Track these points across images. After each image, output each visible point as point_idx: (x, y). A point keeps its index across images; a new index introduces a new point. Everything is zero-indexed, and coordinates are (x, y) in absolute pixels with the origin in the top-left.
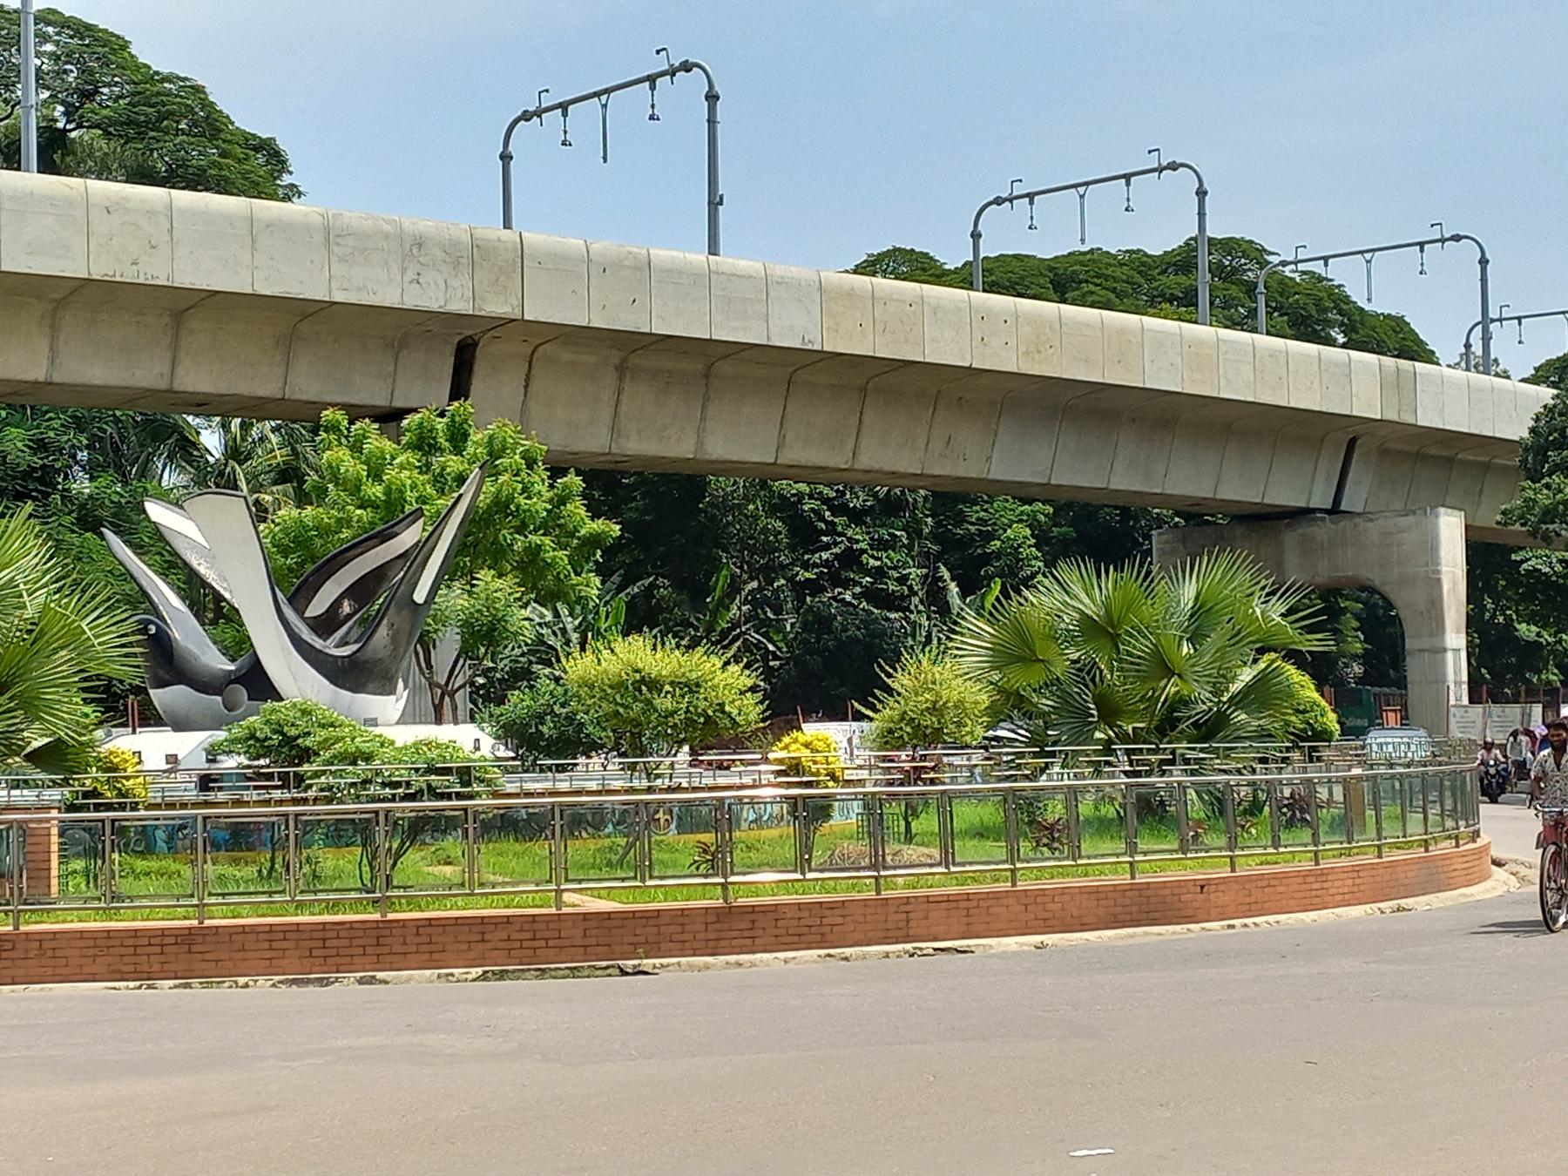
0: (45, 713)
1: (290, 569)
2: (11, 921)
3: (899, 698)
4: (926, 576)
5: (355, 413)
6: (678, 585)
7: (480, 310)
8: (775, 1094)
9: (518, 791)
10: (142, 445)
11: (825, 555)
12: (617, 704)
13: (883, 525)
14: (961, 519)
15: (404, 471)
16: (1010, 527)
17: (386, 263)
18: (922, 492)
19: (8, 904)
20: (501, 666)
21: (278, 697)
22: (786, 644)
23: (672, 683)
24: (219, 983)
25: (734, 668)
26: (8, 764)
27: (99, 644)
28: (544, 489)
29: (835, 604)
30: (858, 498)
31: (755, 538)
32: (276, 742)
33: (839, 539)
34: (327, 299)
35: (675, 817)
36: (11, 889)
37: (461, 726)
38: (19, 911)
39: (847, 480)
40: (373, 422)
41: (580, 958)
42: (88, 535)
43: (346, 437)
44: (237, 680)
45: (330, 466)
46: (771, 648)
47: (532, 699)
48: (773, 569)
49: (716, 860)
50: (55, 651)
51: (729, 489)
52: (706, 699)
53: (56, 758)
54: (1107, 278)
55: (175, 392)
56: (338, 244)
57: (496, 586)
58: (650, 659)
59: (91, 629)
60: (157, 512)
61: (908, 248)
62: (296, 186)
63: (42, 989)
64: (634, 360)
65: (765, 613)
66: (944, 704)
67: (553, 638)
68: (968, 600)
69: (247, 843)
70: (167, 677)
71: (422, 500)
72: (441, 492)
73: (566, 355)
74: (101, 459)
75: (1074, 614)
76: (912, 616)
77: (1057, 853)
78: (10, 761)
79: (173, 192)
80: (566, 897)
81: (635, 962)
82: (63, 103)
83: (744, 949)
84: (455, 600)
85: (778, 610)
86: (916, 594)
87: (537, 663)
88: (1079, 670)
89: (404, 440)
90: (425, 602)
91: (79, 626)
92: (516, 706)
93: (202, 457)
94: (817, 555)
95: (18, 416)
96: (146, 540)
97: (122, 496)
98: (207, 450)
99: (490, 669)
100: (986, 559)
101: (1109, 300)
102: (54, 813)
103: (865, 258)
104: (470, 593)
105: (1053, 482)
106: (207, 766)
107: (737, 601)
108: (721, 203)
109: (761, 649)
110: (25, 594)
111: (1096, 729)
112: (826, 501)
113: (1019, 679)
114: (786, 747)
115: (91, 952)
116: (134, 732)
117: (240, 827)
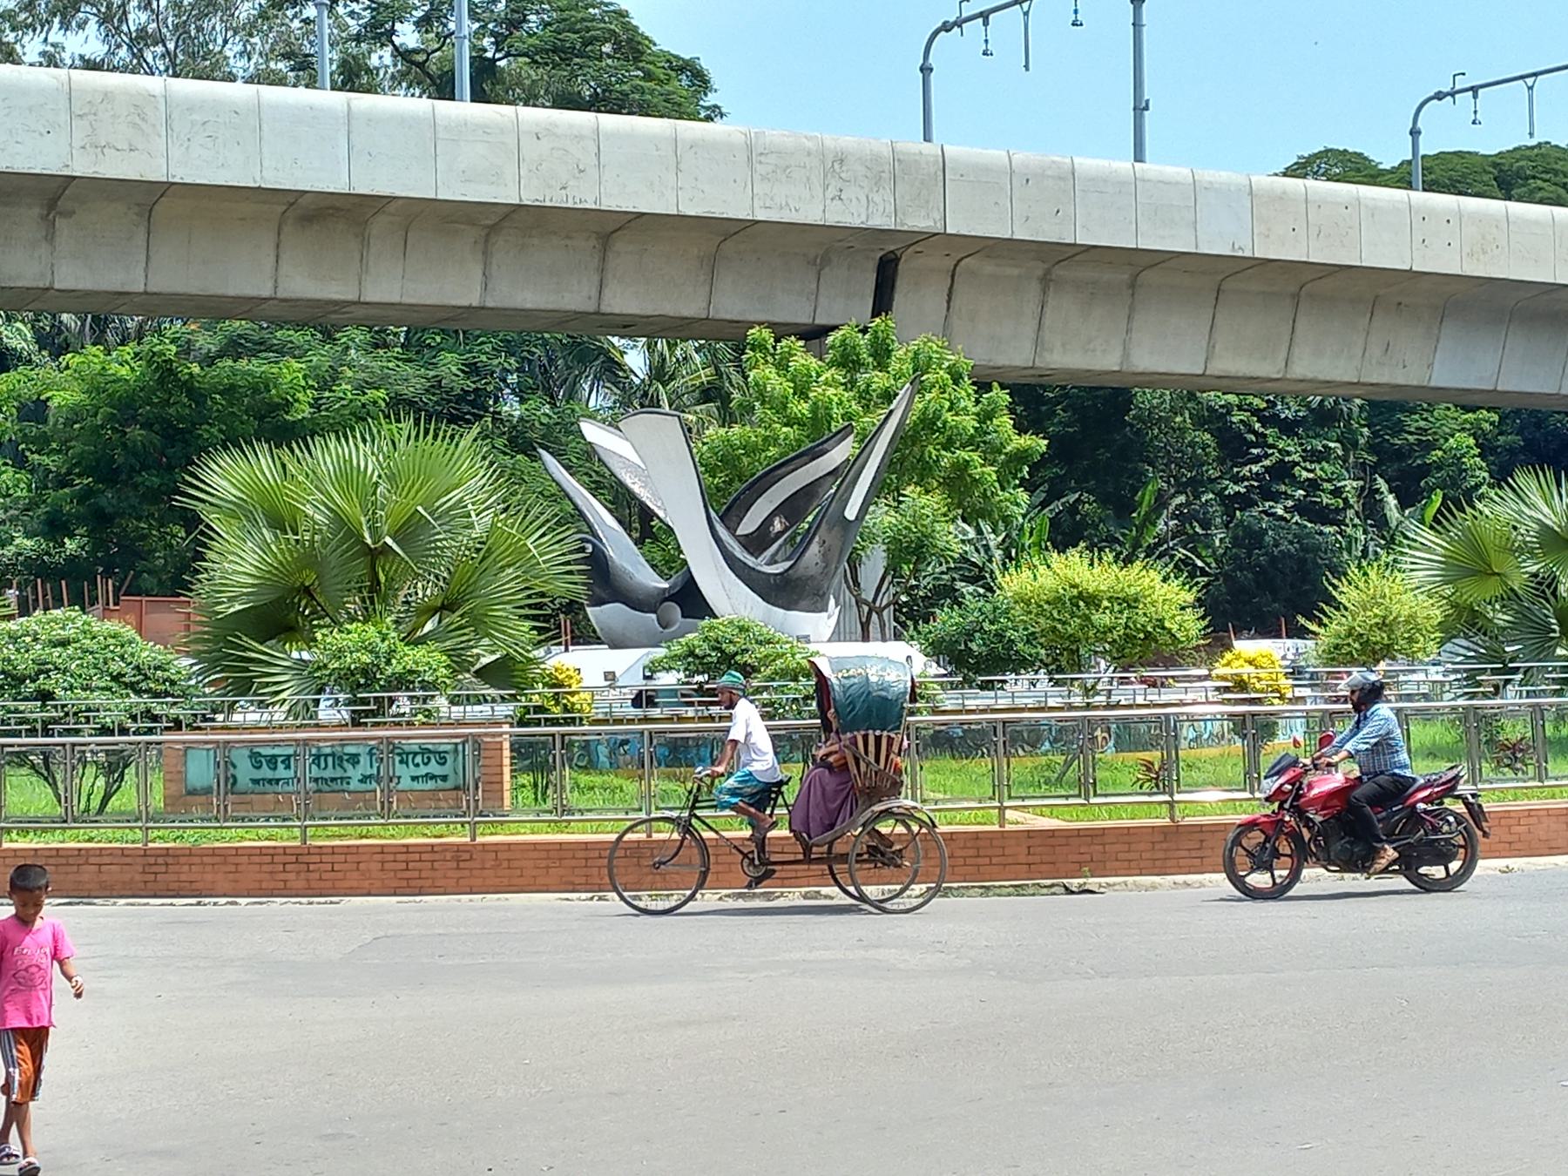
0: (496, 630)
1: (718, 489)
2: (468, 832)
3: (1346, 614)
4: (1363, 488)
5: (781, 331)
6: (1103, 500)
7: (903, 225)
8: (1240, 1015)
9: (960, 708)
10: (569, 368)
11: (1255, 468)
12: (1054, 619)
13: (1317, 436)
14: (1399, 429)
15: (830, 389)
16: (1453, 436)
17: (808, 179)
18: (1358, 401)
19: (464, 816)
20: (925, 582)
21: (716, 617)
22: (1216, 560)
23: (1110, 599)
24: (668, 895)
25: (1175, 584)
26: (459, 681)
27: (544, 562)
28: (970, 405)
29: (1266, 518)
30: (1289, 408)
31: (1182, 451)
32: (715, 660)
33: (1270, 451)
34: (750, 218)
35: (1113, 736)
36: (468, 801)
37: (889, 643)
38: (147, 829)
39: (1275, 391)
40: (798, 339)
41: (1025, 876)
42: (519, 457)
43: (773, 355)
44: (671, 598)
45: (757, 384)
46: (1200, 563)
47: (961, 616)
48: (1201, 483)
49: (1161, 779)
50: (503, 569)
51: (1155, 401)
52: (1145, 614)
53: (505, 674)
54: (1556, 172)
55: (603, 314)
56: (760, 162)
57: (924, 502)
58: (1087, 574)
59: (535, 548)
60: (593, 432)
61: (1341, 149)
62: (719, 108)
63: (499, 899)
64: (1059, 272)
65: (1193, 528)
66: (1396, 618)
67: (976, 555)
68: (1407, 512)
69: (686, 759)
70: (603, 595)
71: (848, 416)
72: (866, 408)
73: (989, 268)
74: (531, 381)
75: (1534, 525)
76: (1348, 530)
77: (1520, 774)
78: (460, 677)
79: (600, 115)
80: (1009, 814)
81: (1081, 881)
82: (493, 34)
83: (1192, 869)
84: (883, 518)
85: (1206, 525)
86: (1351, 507)
87: (961, 581)
88: (1538, 583)
89: (828, 357)
90: (857, 518)
91: (525, 545)
92: (944, 623)
93: (627, 378)
94: (1247, 468)
95: (452, 341)
96: (575, 460)
97: (550, 417)
98: (632, 371)
99: (912, 587)
100: (1425, 470)
101: (1559, 196)
102: (506, 728)
103: (1295, 160)
104: (896, 509)
105: (1499, 388)
106: (644, 682)
107: (1164, 516)
108: (1147, 108)
109: (1189, 565)
110: (473, 514)
111: (1557, 645)
112: (1256, 412)
113: (1476, 593)
114: (1228, 664)
115: (544, 864)
116: (567, 650)
117: (679, 742)
